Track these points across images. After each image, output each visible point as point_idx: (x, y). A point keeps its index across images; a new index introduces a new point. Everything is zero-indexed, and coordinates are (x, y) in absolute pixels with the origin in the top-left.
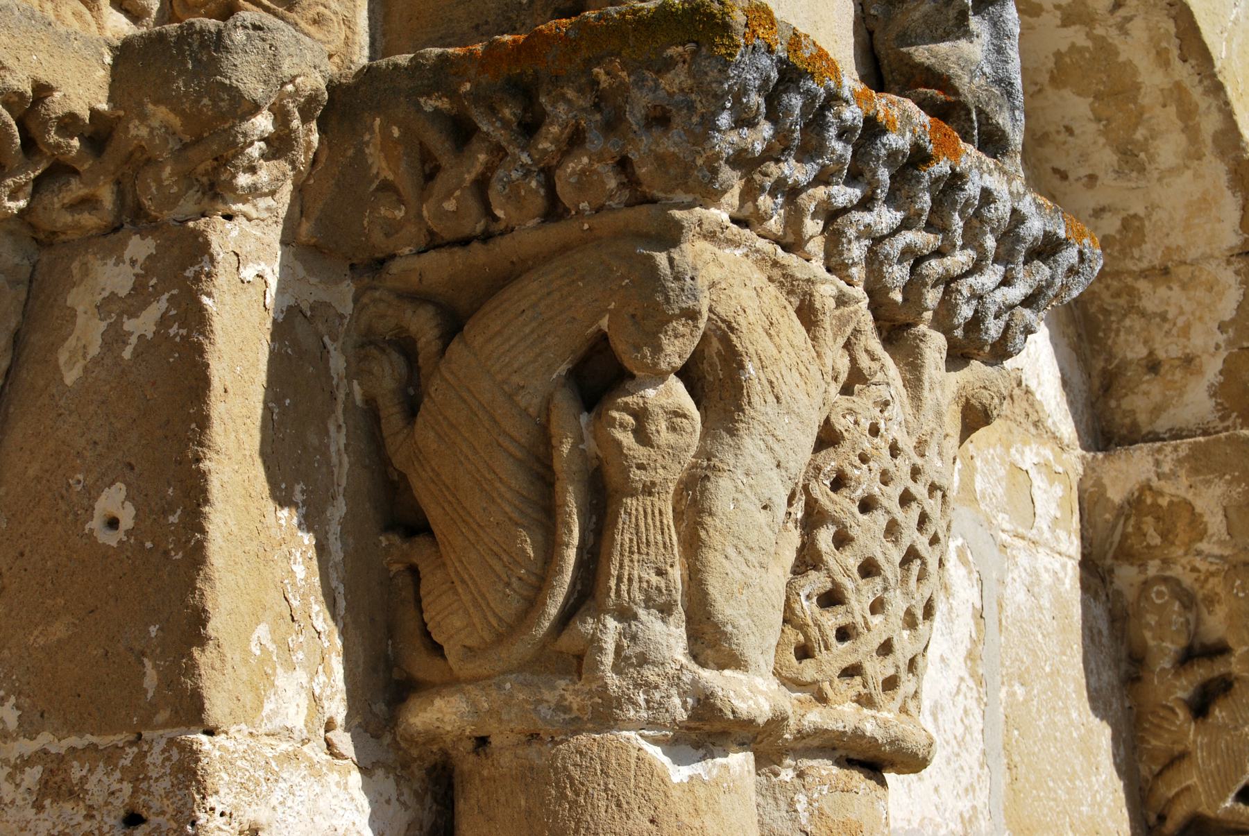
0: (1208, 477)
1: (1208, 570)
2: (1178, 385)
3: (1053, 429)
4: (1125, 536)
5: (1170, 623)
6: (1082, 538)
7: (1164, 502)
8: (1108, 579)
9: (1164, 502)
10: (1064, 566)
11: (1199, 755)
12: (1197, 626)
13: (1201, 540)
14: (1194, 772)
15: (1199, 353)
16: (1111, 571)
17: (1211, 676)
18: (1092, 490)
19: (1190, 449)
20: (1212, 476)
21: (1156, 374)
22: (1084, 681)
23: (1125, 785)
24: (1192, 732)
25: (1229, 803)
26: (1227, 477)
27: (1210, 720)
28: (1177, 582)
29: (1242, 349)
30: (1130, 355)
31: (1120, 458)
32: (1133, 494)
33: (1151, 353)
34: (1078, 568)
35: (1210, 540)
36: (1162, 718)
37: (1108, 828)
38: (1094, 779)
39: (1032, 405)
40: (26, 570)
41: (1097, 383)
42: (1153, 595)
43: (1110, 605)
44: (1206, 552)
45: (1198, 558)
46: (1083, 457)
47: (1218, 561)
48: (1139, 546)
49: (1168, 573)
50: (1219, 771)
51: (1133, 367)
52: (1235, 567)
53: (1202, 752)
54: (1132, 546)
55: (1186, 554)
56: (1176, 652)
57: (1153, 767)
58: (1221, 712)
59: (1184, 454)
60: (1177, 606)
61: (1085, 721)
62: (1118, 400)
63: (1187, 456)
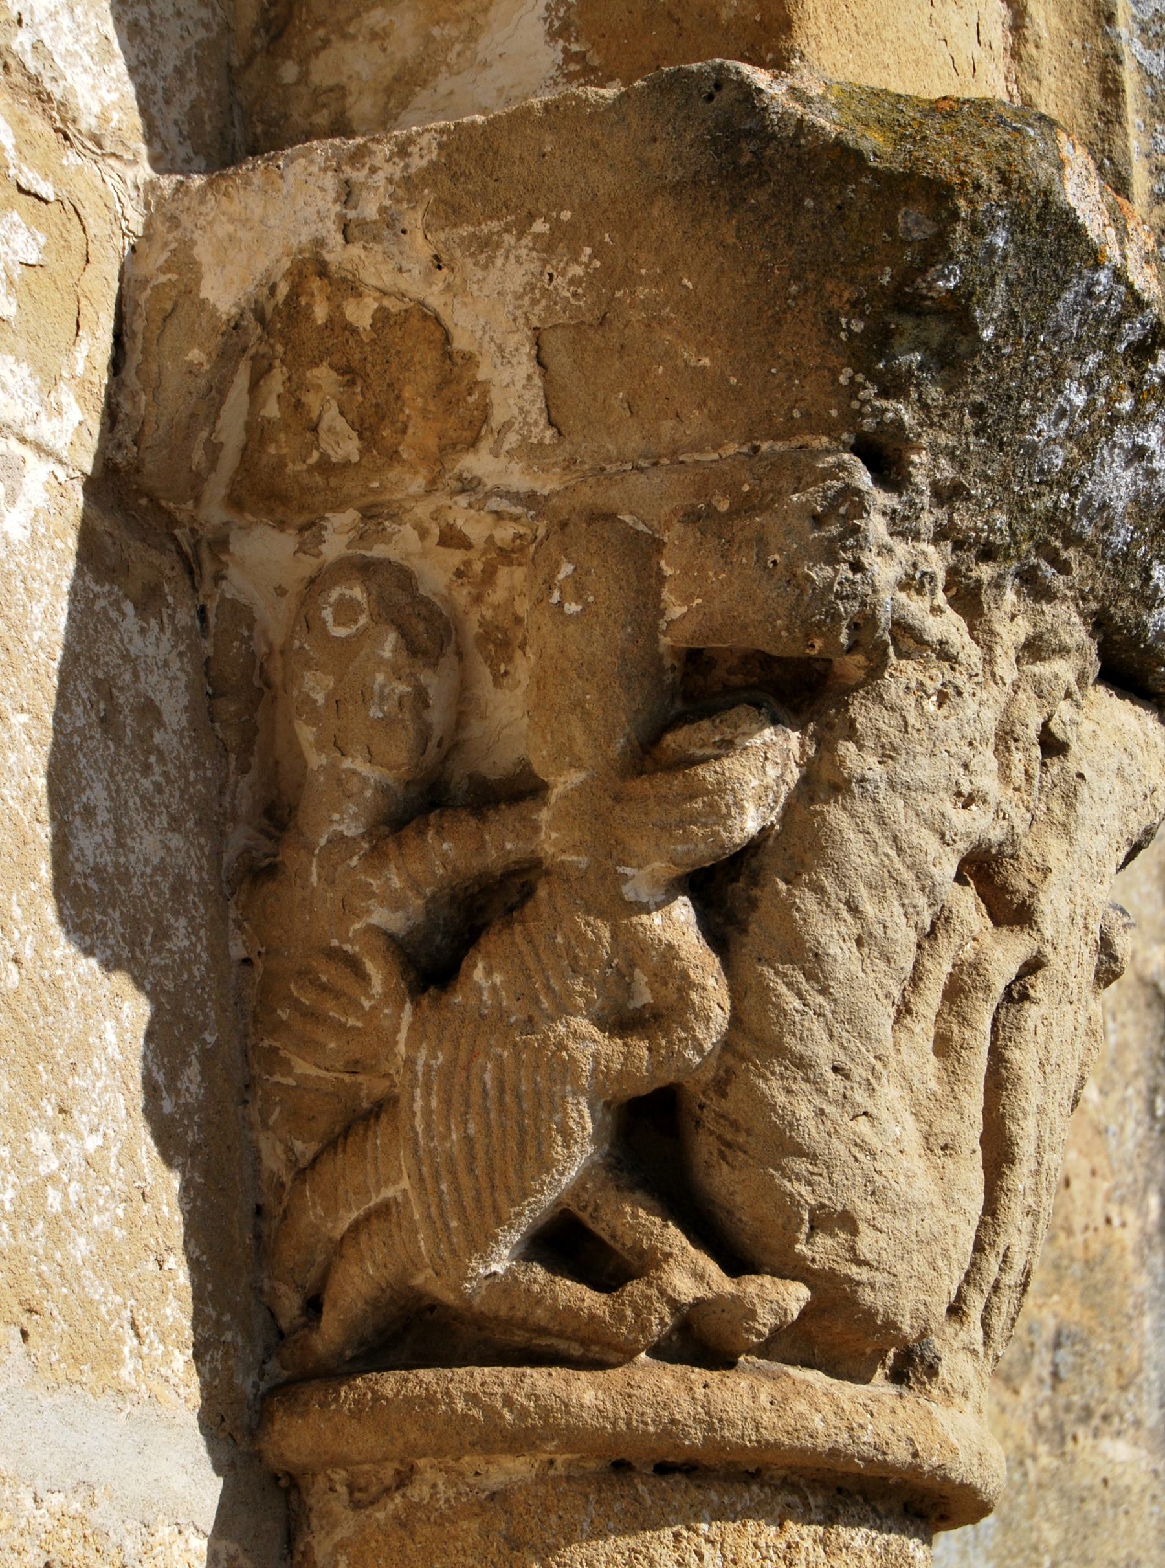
0: (485, 228)
1: (491, 538)
3: (32, 64)
5: (365, 696)
6: (111, 416)
7: (361, 314)
8: (208, 568)
9: (361, 314)
11: (418, 1105)
12: (460, 722)
13: (473, 444)
14: (404, 1159)
16: (220, 544)
18: (163, 279)
19: (441, 146)
20: (495, 225)
22: (44, 833)
23: (185, 1188)
24: (402, 1036)
25: (500, 1263)
27: (459, 999)
28: (405, 578)
31: (248, 183)
32: (273, 289)
34: (78, 497)
35: (498, 443)
36: (324, 988)
37: (87, 1303)
38: (41, 1140)
40: (477, 1474)
42: (327, 614)
44: (490, 484)
45: (463, 501)
46: (152, 186)
47: (518, 510)
49: (378, 551)
50: (472, 1157)
52: (564, 525)
53: (427, 1095)
54: (281, 464)
55: (431, 489)
56: (383, 790)
57: (299, 1146)
58: (489, 972)
59: (424, 163)
60: (389, 645)
61: (28, 953)
62: (303, 61)
63: (434, 166)
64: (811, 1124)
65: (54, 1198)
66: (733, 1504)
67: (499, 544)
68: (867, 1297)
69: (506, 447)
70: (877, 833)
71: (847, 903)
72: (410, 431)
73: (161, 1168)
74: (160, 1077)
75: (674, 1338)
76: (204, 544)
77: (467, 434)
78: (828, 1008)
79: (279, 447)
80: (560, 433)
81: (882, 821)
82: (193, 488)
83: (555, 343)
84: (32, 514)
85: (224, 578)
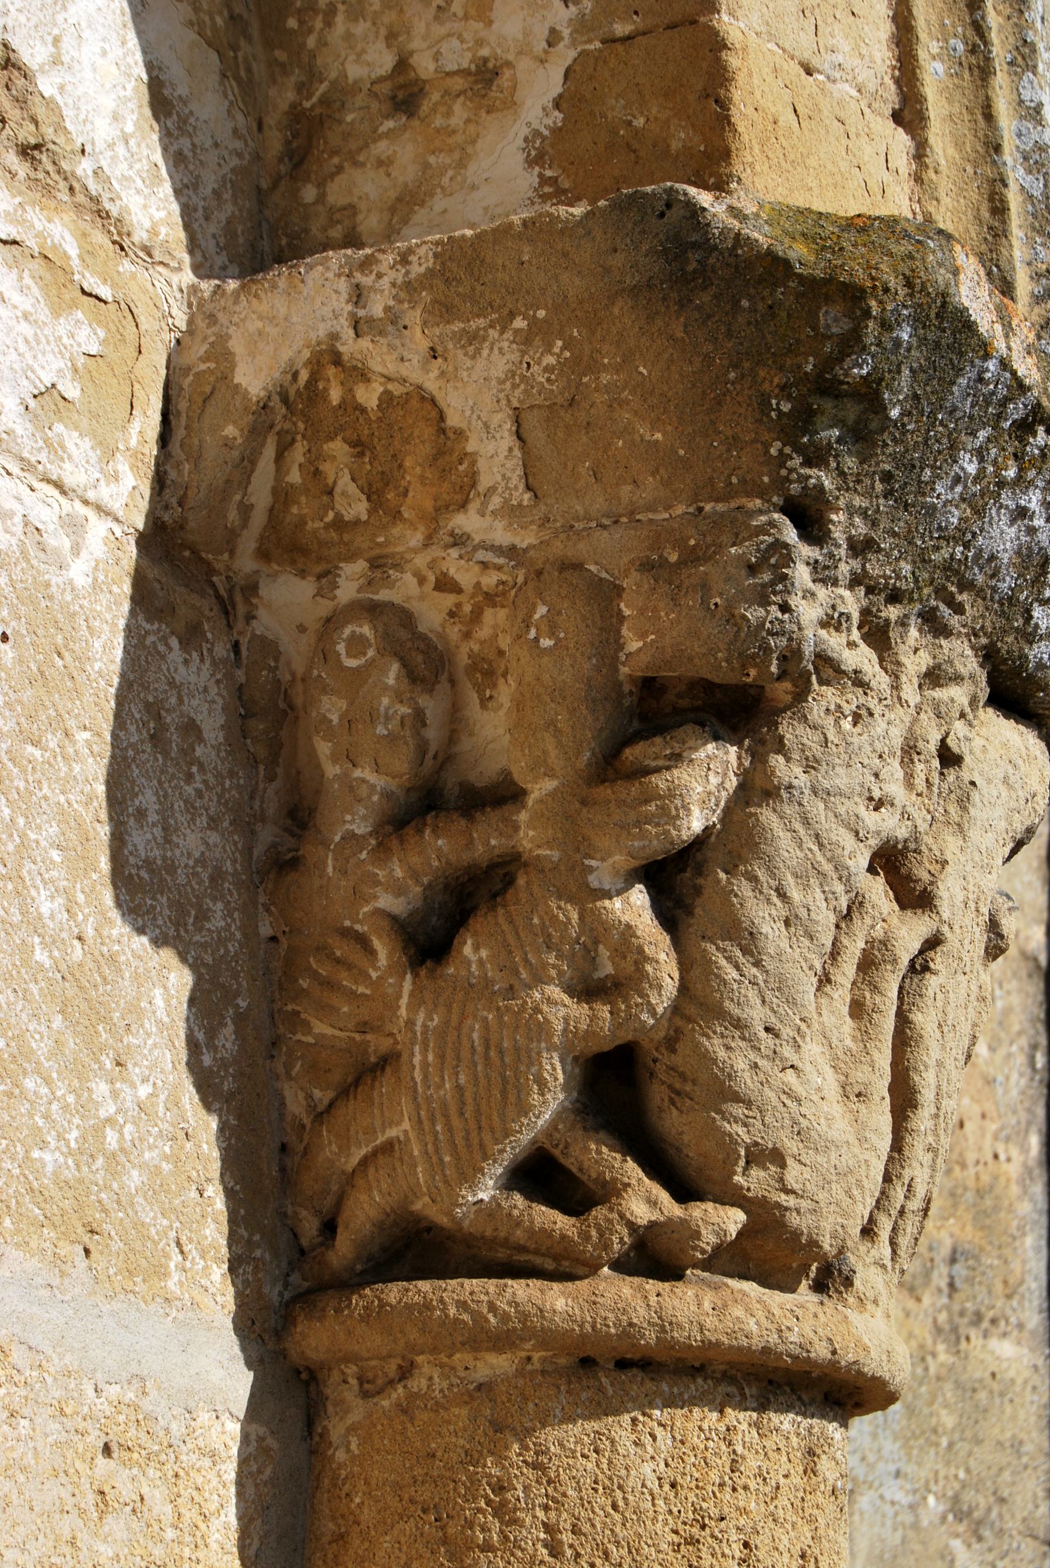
2: (459, 138)
3: (93, 187)
4: (283, 496)
5: (373, 717)
7: (369, 396)
8: (241, 609)
9: (369, 396)
10: (74, 526)
11: (417, 1059)
12: (452, 738)
13: (463, 506)
14: (405, 1105)
15: (511, 57)
16: (251, 589)
17: (466, 857)
18: (203, 367)
19: (436, 256)
20: (481, 322)
21: (411, 115)
22: (104, 831)
23: (222, 1129)
24: (404, 1001)
25: (486, 1192)
26: (519, 323)
28: (406, 618)
29: (610, 41)
30: (354, 71)
31: (274, 286)
32: (295, 375)
33: (402, 65)
35: (485, 504)
36: (338, 961)
38: (101, 1088)
39: (21, 102)
41: (275, 142)
42: (341, 648)
43: (240, 675)
44: (477, 539)
45: (454, 553)
46: (194, 289)
47: (501, 561)
48: (318, 524)
49: (384, 595)
50: (462, 1103)
51: (360, 100)
52: (539, 573)
53: (425, 1051)
54: (302, 522)
57: (317, 1093)
58: (476, 948)
60: (393, 673)
62: (321, 185)
63: (430, 273)
64: (747, 1075)
65: (111, 1137)
66: (681, 1394)
67: (485, 589)
68: (794, 1220)
69: (491, 507)
70: (802, 832)
71: (777, 890)
72: (411, 495)
73: (202, 1112)
74: (200, 1036)
75: (632, 1254)
76: (238, 589)
77: (458, 497)
78: (760, 978)
79: (300, 508)
80: (536, 496)
81: (806, 822)
82: (228, 542)
83: (531, 420)
84: (93, 564)
85: (254, 617)
